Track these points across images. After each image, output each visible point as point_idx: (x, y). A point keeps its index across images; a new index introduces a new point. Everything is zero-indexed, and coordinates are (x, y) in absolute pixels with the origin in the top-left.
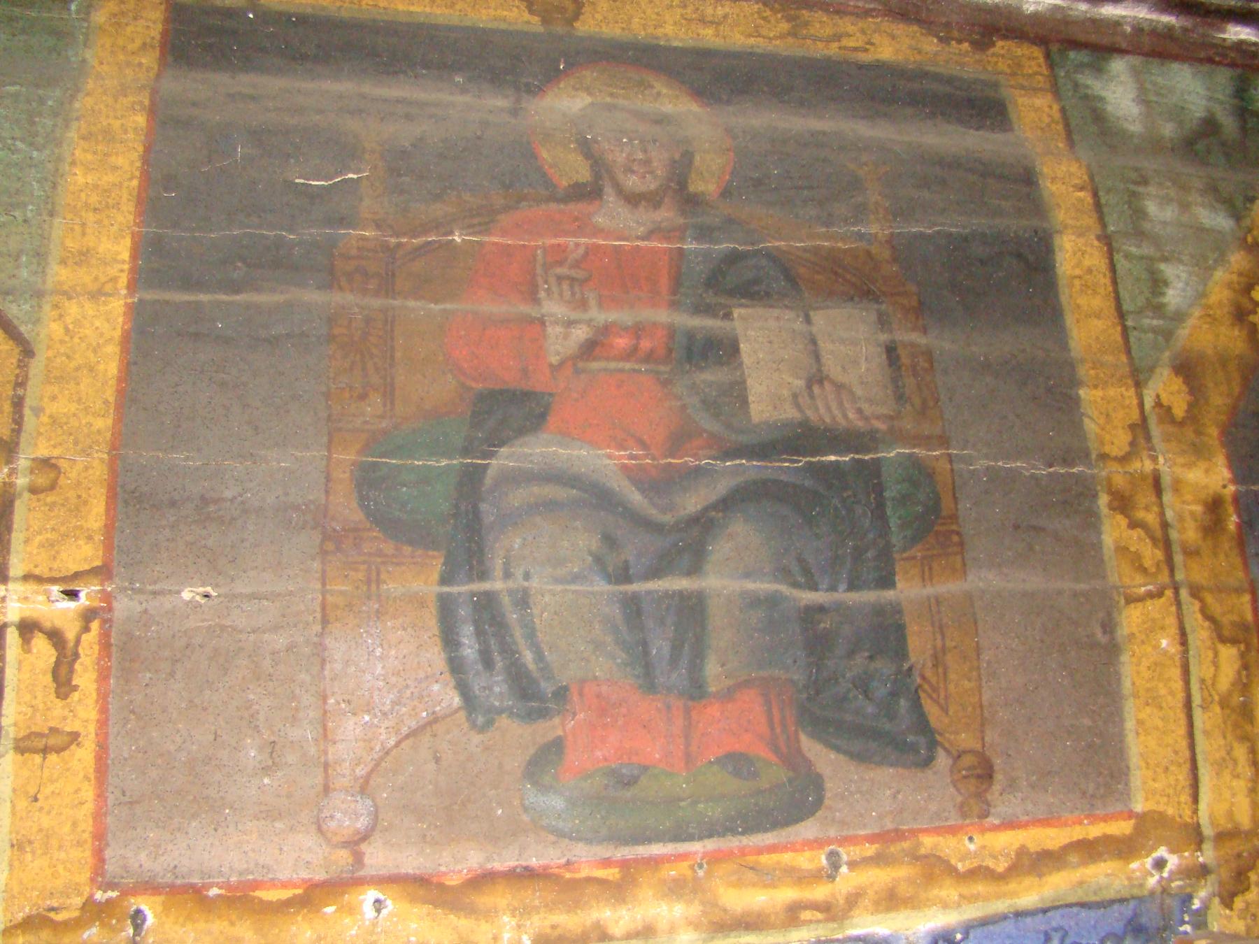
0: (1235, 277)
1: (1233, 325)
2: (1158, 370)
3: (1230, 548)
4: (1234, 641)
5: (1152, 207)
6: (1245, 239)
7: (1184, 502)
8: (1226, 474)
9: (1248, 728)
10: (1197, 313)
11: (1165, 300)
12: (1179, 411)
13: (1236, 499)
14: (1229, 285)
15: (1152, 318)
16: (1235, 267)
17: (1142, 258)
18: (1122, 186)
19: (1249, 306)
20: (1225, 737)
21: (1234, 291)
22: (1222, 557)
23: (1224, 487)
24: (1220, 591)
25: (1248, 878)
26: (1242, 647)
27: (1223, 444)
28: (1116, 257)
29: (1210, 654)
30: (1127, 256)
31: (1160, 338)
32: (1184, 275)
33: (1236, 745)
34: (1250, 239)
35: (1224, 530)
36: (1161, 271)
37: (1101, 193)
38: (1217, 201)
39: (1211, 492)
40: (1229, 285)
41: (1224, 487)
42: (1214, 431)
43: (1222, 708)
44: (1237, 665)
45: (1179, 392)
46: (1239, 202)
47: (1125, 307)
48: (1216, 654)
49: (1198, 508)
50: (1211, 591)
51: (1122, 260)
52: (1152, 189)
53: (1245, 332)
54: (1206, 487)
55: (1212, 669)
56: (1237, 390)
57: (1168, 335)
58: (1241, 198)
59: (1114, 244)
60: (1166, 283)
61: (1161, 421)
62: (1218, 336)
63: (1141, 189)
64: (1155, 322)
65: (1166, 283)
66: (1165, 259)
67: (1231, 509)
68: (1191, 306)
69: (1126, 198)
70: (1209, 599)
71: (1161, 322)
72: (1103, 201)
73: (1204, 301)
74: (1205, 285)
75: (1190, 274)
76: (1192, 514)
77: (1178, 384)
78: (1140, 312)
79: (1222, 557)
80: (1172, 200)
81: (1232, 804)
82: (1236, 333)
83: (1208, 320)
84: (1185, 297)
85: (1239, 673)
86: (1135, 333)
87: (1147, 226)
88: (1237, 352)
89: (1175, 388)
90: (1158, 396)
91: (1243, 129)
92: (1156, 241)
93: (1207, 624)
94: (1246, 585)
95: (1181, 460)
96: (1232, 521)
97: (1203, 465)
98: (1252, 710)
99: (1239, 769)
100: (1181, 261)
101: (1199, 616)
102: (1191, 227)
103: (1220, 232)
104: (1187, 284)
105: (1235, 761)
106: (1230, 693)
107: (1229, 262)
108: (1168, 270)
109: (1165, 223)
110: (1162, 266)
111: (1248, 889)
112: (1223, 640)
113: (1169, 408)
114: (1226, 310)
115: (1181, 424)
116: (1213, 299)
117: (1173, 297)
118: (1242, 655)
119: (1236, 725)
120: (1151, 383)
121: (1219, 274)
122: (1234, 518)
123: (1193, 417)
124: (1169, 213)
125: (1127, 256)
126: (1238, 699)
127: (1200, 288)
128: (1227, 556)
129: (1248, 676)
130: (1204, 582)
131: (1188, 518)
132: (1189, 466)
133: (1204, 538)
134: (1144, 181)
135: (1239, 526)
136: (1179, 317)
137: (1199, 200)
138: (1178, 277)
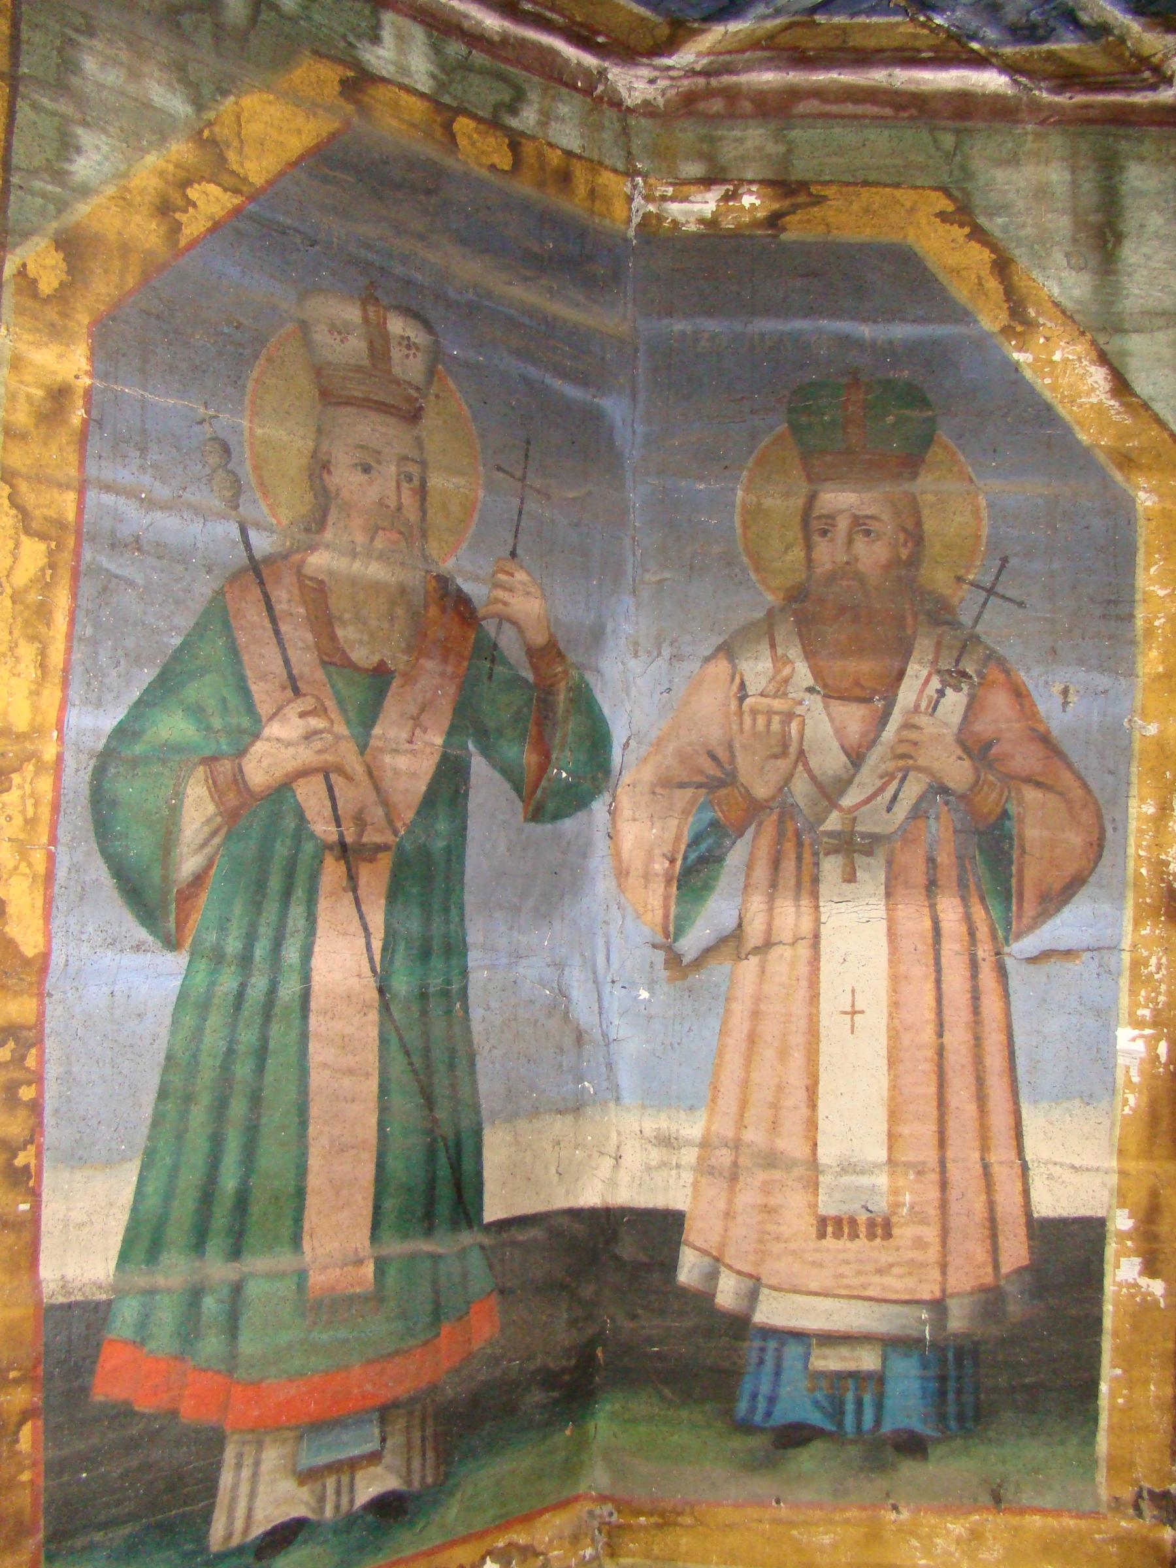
0: (171, 168)
1: (152, 216)
2: (36, 239)
3: (68, 443)
4: (42, 537)
5: (90, 64)
6: (201, 132)
7: (22, 382)
8: (84, 365)
9: (43, 629)
10: (110, 190)
11: (72, 168)
12: (48, 284)
13: (88, 393)
14: (162, 174)
15: (48, 183)
16: (174, 157)
17: (54, 114)
18: (57, 28)
19: (180, 202)
20: (11, 633)
21: (167, 182)
22: (54, 448)
23: (77, 377)
24: (40, 481)
25: (11, 780)
26: (53, 545)
27: (91, 335)
28: (20, 103)
29: (11, 544)
30: (35, 106)
31: (51, 207)
32: (105, 149)
33: (22, 642)
34: (206, 134)
35: (65, 422)
36: (77, 136)
37: (23, 27)
38: (179, 81)
39: (59, 378)
40: (162, 174)
41: (77, 377)
42: (85, 319)
43: (14, 602)
44: (42, 561)
45: (53, 268)
46: (206, 91)
47: (15, 161)
48: (17, 545)
49: (39, 393)
50: (27, 478)
51: (28, 109)
52: (97, 44)
53: (163, 229)
54: (55, 373)
55: (10, 560)
56: (130, 283)
57: (62, 206)
58: (212, 87)
59: (21, 88)
60: (78, 150)
61: (19, 291)
62: (128, 223)
63: (82, 39)
64: (50, 188)
65: (78, 150)
66: (85, 124)
67: (80, 403)
68: (104, 183)
69: (58, 43)
70: (23, 487)
71: (59, 190)
72: (24, 36)
73: (122, 182)
74: (130, 166)
75: (113, 149)
76: (29, 397)
77: (55, 259)
78: (34, 172)
79: (54, 448)
80: (121, 64)
81: (9, 703)
82: (154, 226)
83: (121, 203)
84: (99, 172)
85: (42, 570)
86: (19, 192)
87: (75, 81)
88: (148, 246)
89: (50, 262)
90: (24, 265)
91: (253, 20)
92: (80, 101)
93: (14, 512)
94: (76, 484)
95: (27, 337)
96: (78, 415)
97: (56, 348)
98: (51, 612)
99: (22, 667)
100: (104, 131)
101: (6, 502)
102: (136, 100)
103: (170, 115)
104: (107, 158)
105: (18, 660)
106: (26, 589)
107: (168, 150)
108: (86, 137)
109: (101, 86)
110: (80, 131)
111: (8, 790)
112: (28, 531)
113: (34, 282)
114: (147, 199)
115: (48, 300)
116: (136, 182)
117: (82, 168)
118: (51, 553)
119: (27, 623)
120: (18, 251)
121: (151, 159)
122: (81, 412)
123: (62, 297)
124: (113, 77)
125: (35, 106)
126: (34, 597)
127: (123, 167)
128: (61, 449)
129: (52, 577)
130: (24, 470)
131: (22, 399)
132: (38, 345)
133: (37, 426)
134: (91, 32)
135: (85, 423)
136: (84, 191)
137: (157, 74)
138: (98, 148)
